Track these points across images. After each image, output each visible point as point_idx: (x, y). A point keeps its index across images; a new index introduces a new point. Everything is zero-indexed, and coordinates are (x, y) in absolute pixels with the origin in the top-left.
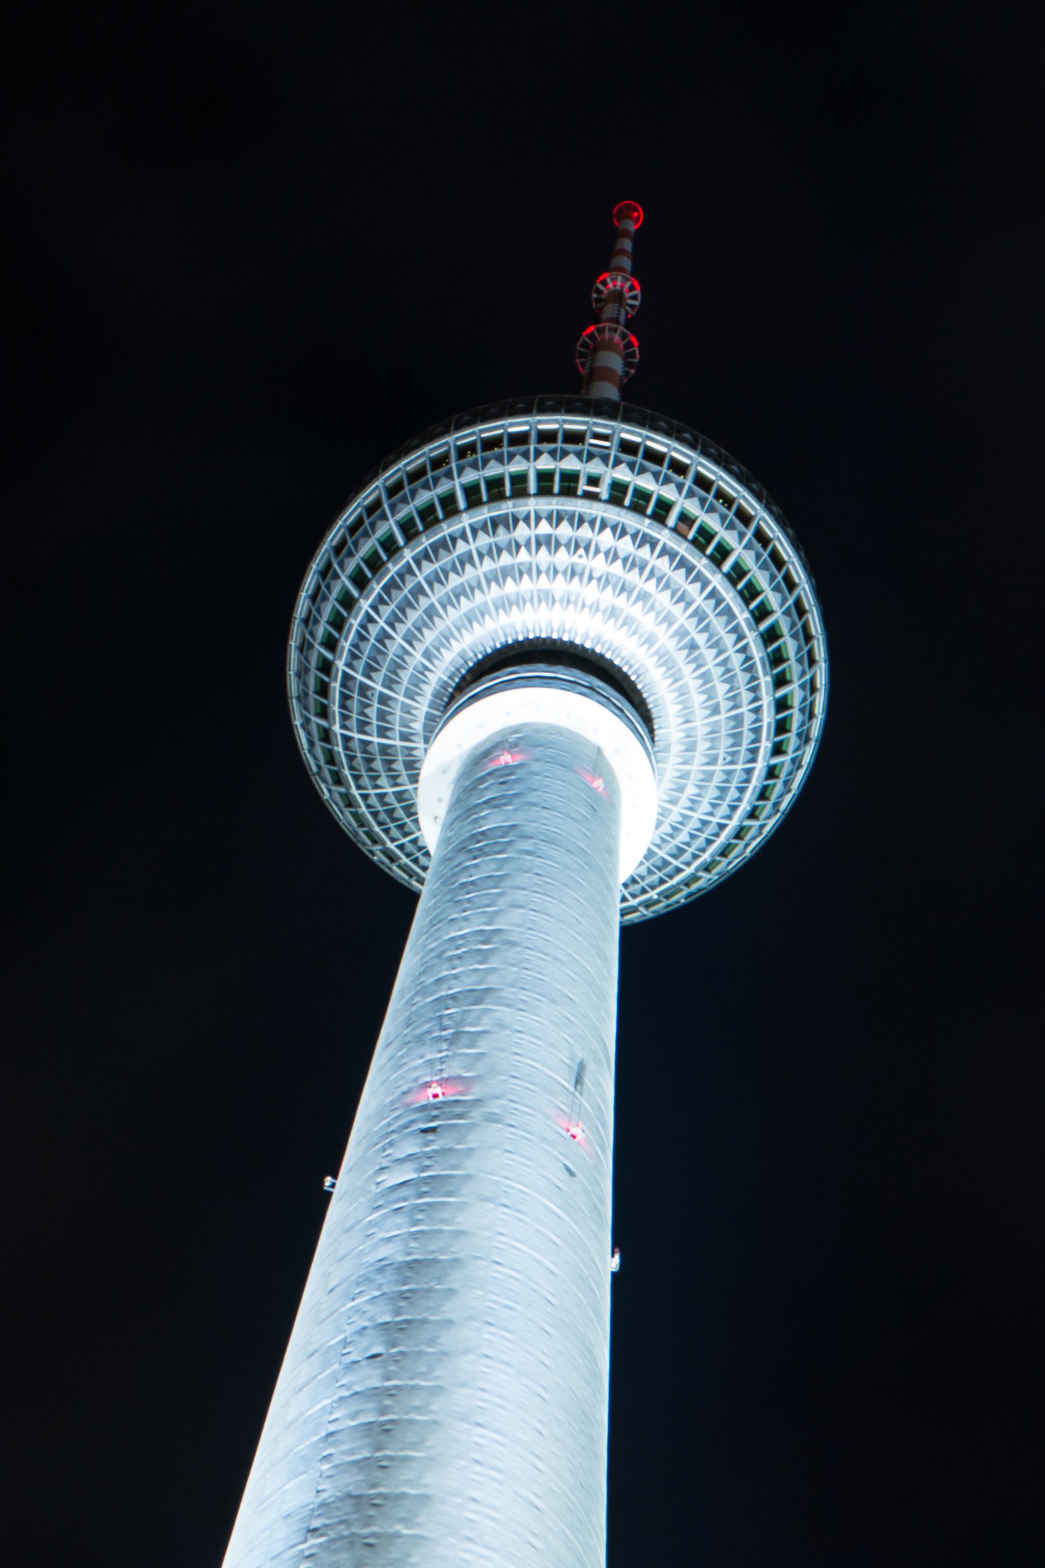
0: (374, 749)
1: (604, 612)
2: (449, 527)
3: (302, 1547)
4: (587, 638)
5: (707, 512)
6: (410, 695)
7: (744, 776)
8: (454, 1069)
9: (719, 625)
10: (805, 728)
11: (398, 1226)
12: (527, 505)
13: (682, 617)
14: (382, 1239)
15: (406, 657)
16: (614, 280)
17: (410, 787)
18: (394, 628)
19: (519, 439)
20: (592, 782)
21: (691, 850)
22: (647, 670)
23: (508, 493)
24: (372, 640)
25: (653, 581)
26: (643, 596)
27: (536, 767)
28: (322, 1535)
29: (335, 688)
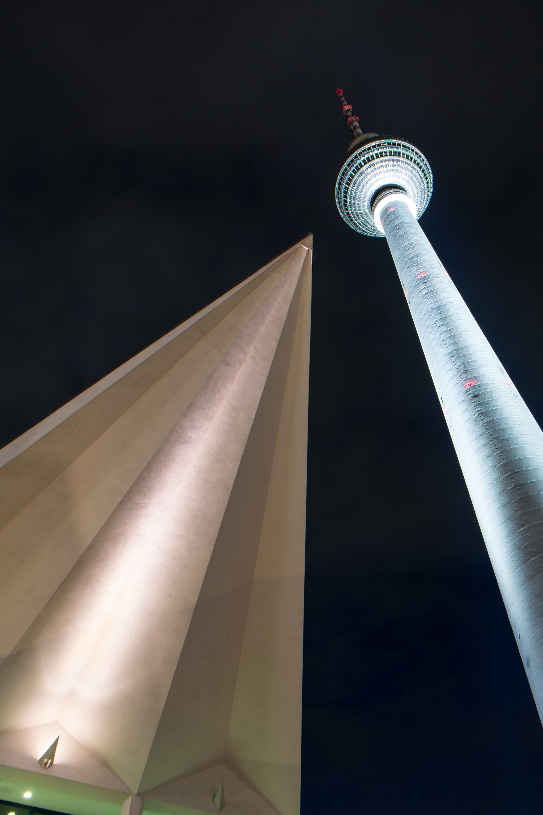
1: (385, 166)
3: (451, 360)
6: (363, 202)
8: (421, 270)
9: (415, 172)
11: (430, 301)
13: (408, 173)
14: (429, 304)
15: (361, 195)
16: (347, 107)
19: (369, 149)
24: (354, 194)
25: (402, 168)
27: (398, 209)
28: (454, 357)
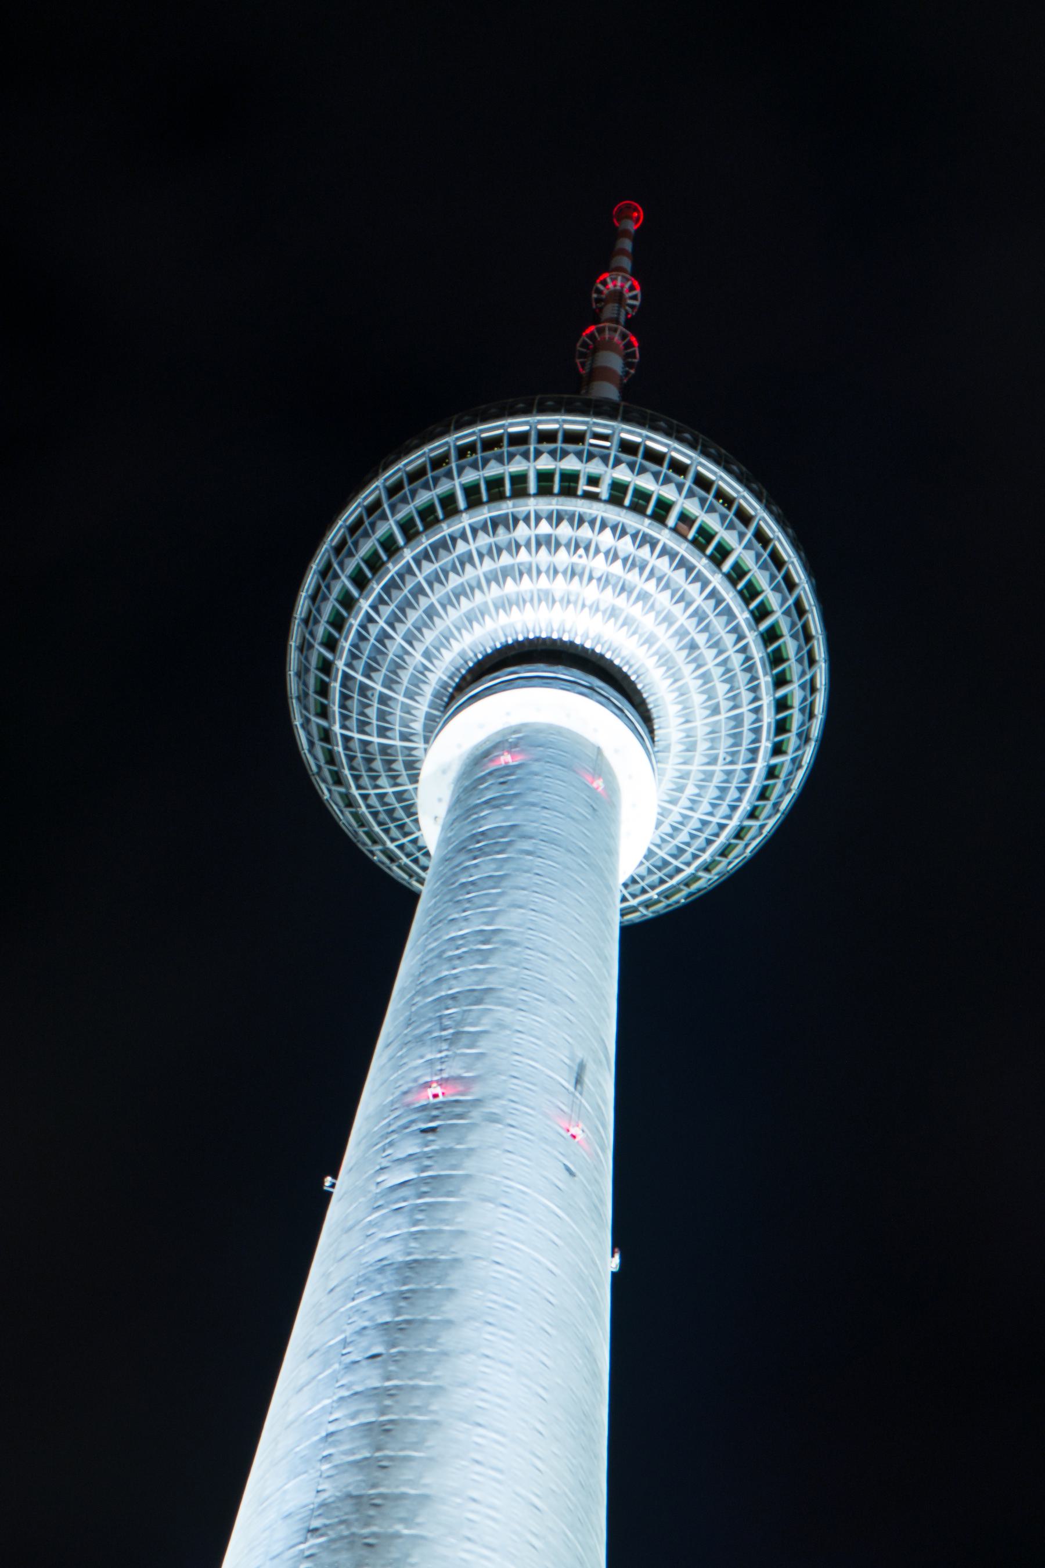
0: (374, 749)
1: (604, 612)
2: (449, 527)
3: (302, 1547)
4: (587, 638)
5: (707, 512)
6: (410, 695)
7: (744, 776)
8: (454, 1069)
9: (719, 625)
10: (805, 728)
11: (398, 1226)
12: (527, 505)
13: (682, 617)
14: (382, 1239)
15: (406, 657)
16: (614, 280)
17: (410, 787)
18: (394, 628)
19: (519, 439)
20: (592, 782)
21: (691, 850)
22: (647, 670)
23: (508, 493)
24: (372, 640)
25: (653, 581)
26: (643, 596)
27: (536, 767)
28: (322, 1535)
29: (335, 688)
